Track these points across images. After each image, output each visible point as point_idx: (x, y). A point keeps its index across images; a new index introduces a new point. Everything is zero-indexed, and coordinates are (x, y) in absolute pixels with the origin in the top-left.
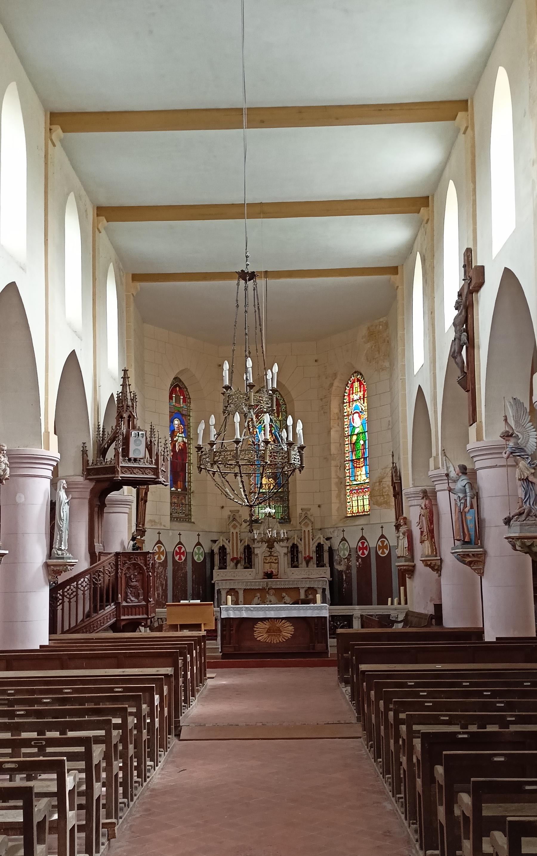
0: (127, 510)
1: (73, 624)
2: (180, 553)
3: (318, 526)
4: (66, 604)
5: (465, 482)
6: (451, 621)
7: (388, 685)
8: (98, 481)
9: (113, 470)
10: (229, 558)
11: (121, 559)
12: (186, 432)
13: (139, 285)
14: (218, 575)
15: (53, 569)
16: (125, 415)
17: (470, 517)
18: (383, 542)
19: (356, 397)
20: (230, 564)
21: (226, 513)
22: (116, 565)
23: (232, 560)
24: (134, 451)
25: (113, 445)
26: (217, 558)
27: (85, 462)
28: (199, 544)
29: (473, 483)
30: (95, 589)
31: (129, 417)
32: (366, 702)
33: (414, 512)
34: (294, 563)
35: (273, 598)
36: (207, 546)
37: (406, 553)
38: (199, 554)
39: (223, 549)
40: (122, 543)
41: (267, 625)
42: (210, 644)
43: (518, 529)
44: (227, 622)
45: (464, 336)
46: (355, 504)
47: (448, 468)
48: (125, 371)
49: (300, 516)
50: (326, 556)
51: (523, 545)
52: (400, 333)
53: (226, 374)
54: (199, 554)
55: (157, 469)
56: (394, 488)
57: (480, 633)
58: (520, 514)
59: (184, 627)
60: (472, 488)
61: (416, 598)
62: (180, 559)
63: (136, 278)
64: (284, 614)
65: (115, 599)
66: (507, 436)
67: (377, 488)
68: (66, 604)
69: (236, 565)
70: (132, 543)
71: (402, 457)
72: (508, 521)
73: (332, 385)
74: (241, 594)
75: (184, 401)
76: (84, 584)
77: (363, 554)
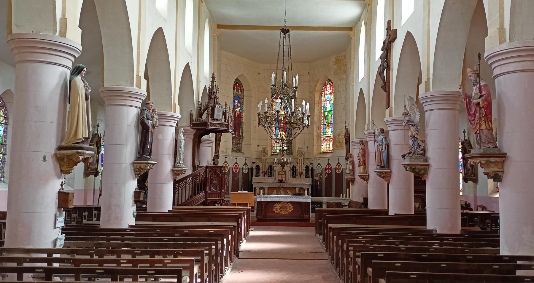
0: (211, 145)
1: (183, 201)
2: (236, 168)
3: (306, 157)
4: (180, 191)
5: (383, 137)
6: (371, 206)
7: (344, 233)
8: (198, 129)
9: (206, 124)
10: (260, 172)
11: (208, 169)
12: (241, 106)
13: (220, 30)
14: (255, 180)
15: (175, 172)
16: (213, 97)
17: (385, 154)
18: (339, 166)
19: (328, 92)
20: (261, 175)
21: (260, 149)
22: (206, 172)
23: (262, 172)
24: (217, 115)
25: (206, 112)
26: (255, 171)
27: (191, 120)
28: (246, 164)
29: (386, 138)
30: (195, 184)
31: (215, 98)
32: (331, 241)
33: (355, 152)
34: (294, 175)
35: (282, 192)
36: (250, 165)
37: (351, 172)
38: (245, 169)
39: (258, 167)
40: (208, 161)
41: (280, 205)
42: (252, 214)
43: (408, 160)
44: (260, 203)
45: (385, 65)
46: (325, 146)
47: (374, 130)
48: (213, 74)
49: (298, 152)
50: (310, 172)
51: (411, 168)
52: (352, 61)
53: (273, 78)
54: (245, 169)
55: (228, 124)
56: (346, 139)
57: (387, 212)
58: (410, 153)
59: (239, 204)
60: (386, 140)
61: (355, 194)
62: (236, 171)
63: (219, 27)
64: (289, 200)
65: (205, 190)
66: (405, 114)
67: (337, 139)
68: (180, 191)
69: (264, 175)
70: (213, 162)
71: (350, 123)
72: (404, 156)
73: (316, 85)
74: (266, 189)
75: (241, 91)
76: (190, 181)
77: (329, 172)
